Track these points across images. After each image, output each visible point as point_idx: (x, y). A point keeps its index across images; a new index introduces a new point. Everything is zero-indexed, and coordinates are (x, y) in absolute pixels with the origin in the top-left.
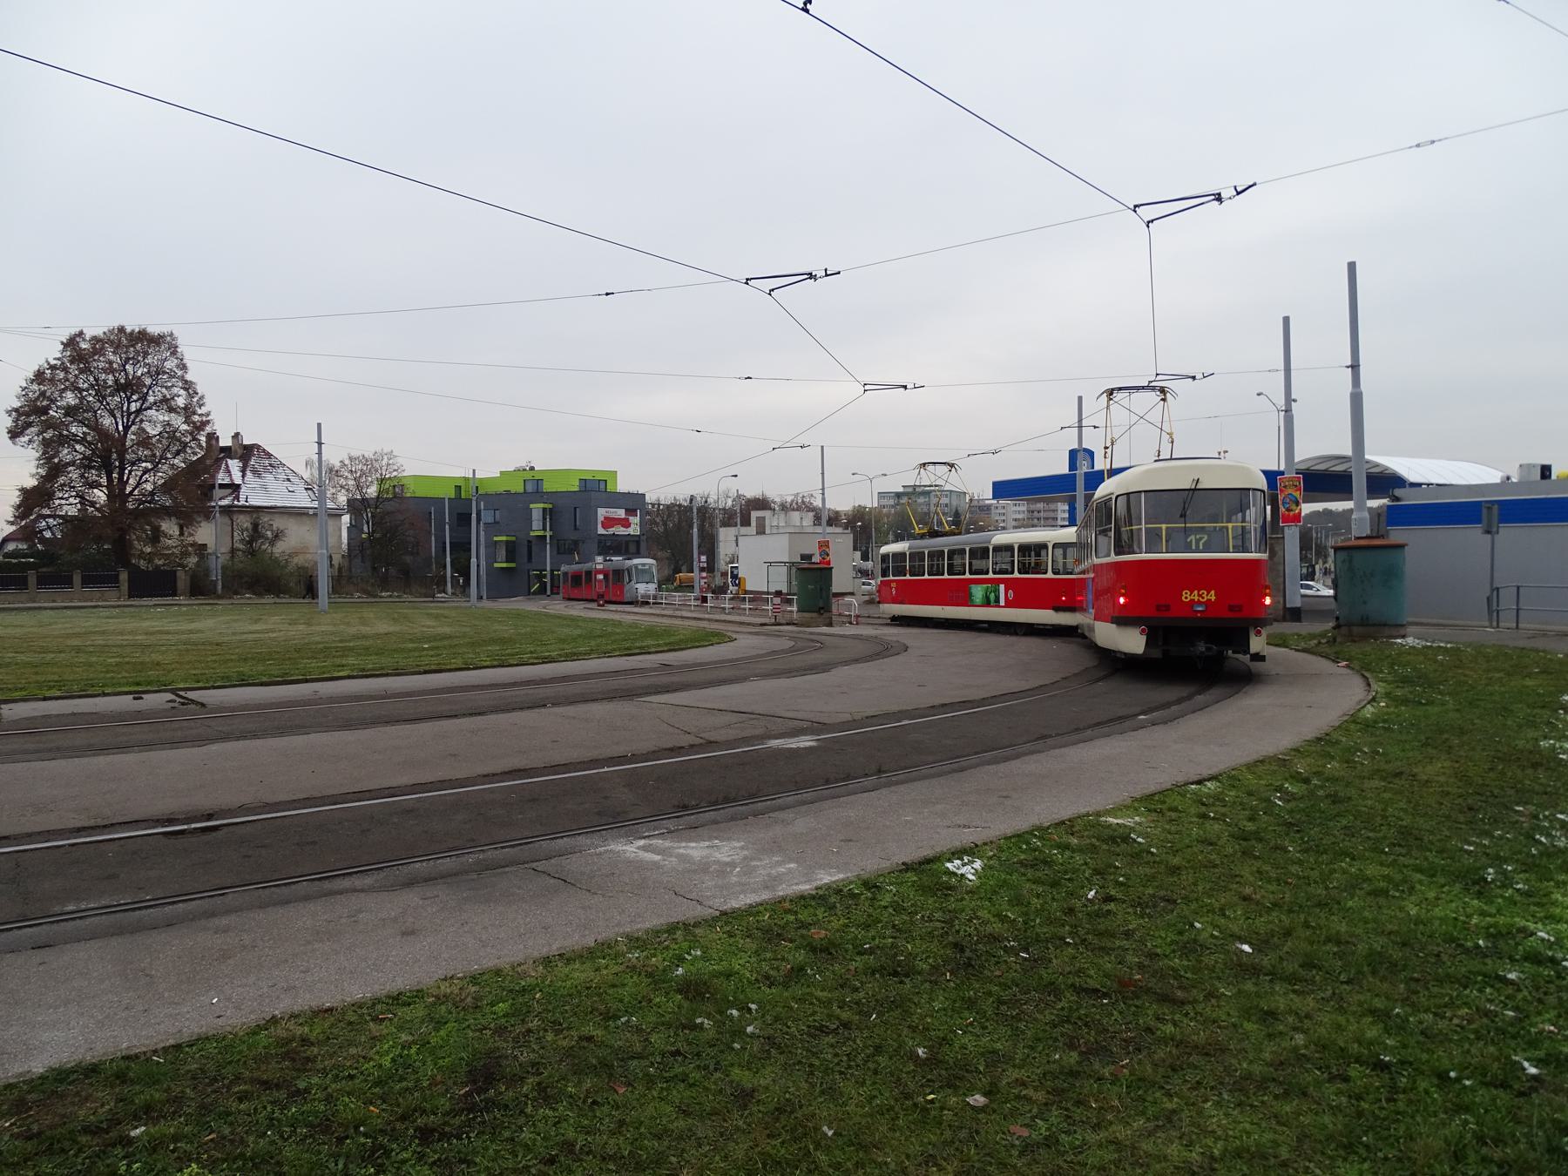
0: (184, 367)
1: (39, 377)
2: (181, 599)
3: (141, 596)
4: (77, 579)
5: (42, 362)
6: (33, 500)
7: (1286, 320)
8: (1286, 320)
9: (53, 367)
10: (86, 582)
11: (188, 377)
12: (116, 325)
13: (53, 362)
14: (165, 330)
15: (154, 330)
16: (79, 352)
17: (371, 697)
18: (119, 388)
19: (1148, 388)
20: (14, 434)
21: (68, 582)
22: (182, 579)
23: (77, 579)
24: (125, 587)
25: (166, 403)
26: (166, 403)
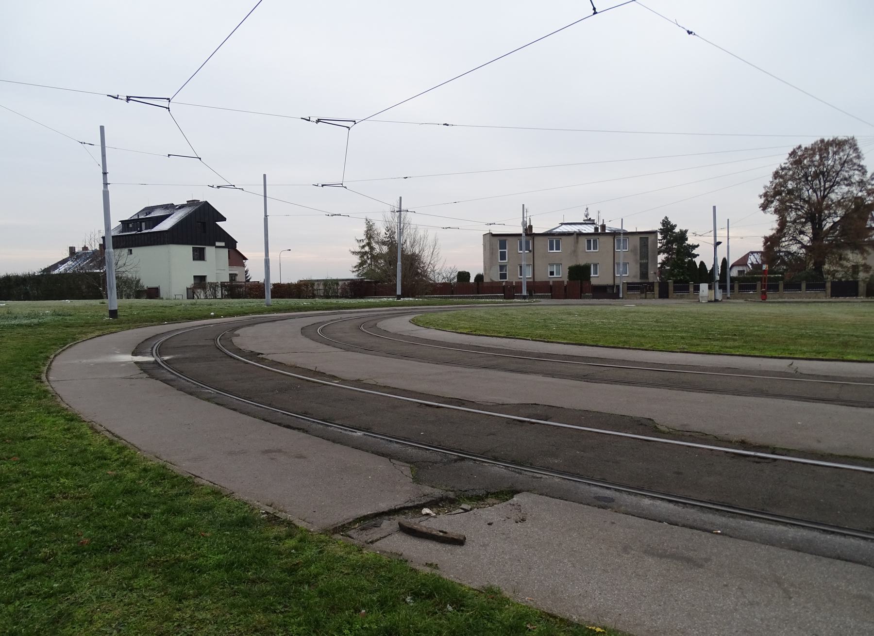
0: (859, 157)
1: (776, 175)
2: (862, 298)
3: (838, 296)
4: (804, 286)
5: (778, 166)
6: (772, 242)
7: (714, 207)
8: (714, 207)
9: (783, 169)
10: (808, 287)
11: (862, 163)
12: (819, 139)
13: (783, 166)
14: (850, 135)
15: (841, 137)
16: (797, 158)
17: (818, 377)
18: (816, 175)
19: (715, 249)
20: (764, 207)
21: (800, 288)
22: (862, 287)
23: (804, 286)
24: (829, 291)
25: (848, 181)
26: (848, 181)
